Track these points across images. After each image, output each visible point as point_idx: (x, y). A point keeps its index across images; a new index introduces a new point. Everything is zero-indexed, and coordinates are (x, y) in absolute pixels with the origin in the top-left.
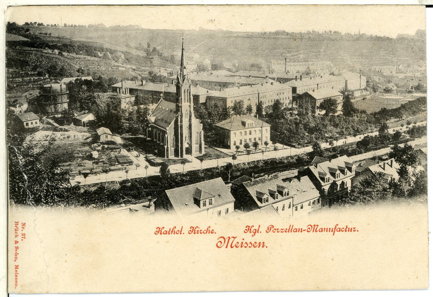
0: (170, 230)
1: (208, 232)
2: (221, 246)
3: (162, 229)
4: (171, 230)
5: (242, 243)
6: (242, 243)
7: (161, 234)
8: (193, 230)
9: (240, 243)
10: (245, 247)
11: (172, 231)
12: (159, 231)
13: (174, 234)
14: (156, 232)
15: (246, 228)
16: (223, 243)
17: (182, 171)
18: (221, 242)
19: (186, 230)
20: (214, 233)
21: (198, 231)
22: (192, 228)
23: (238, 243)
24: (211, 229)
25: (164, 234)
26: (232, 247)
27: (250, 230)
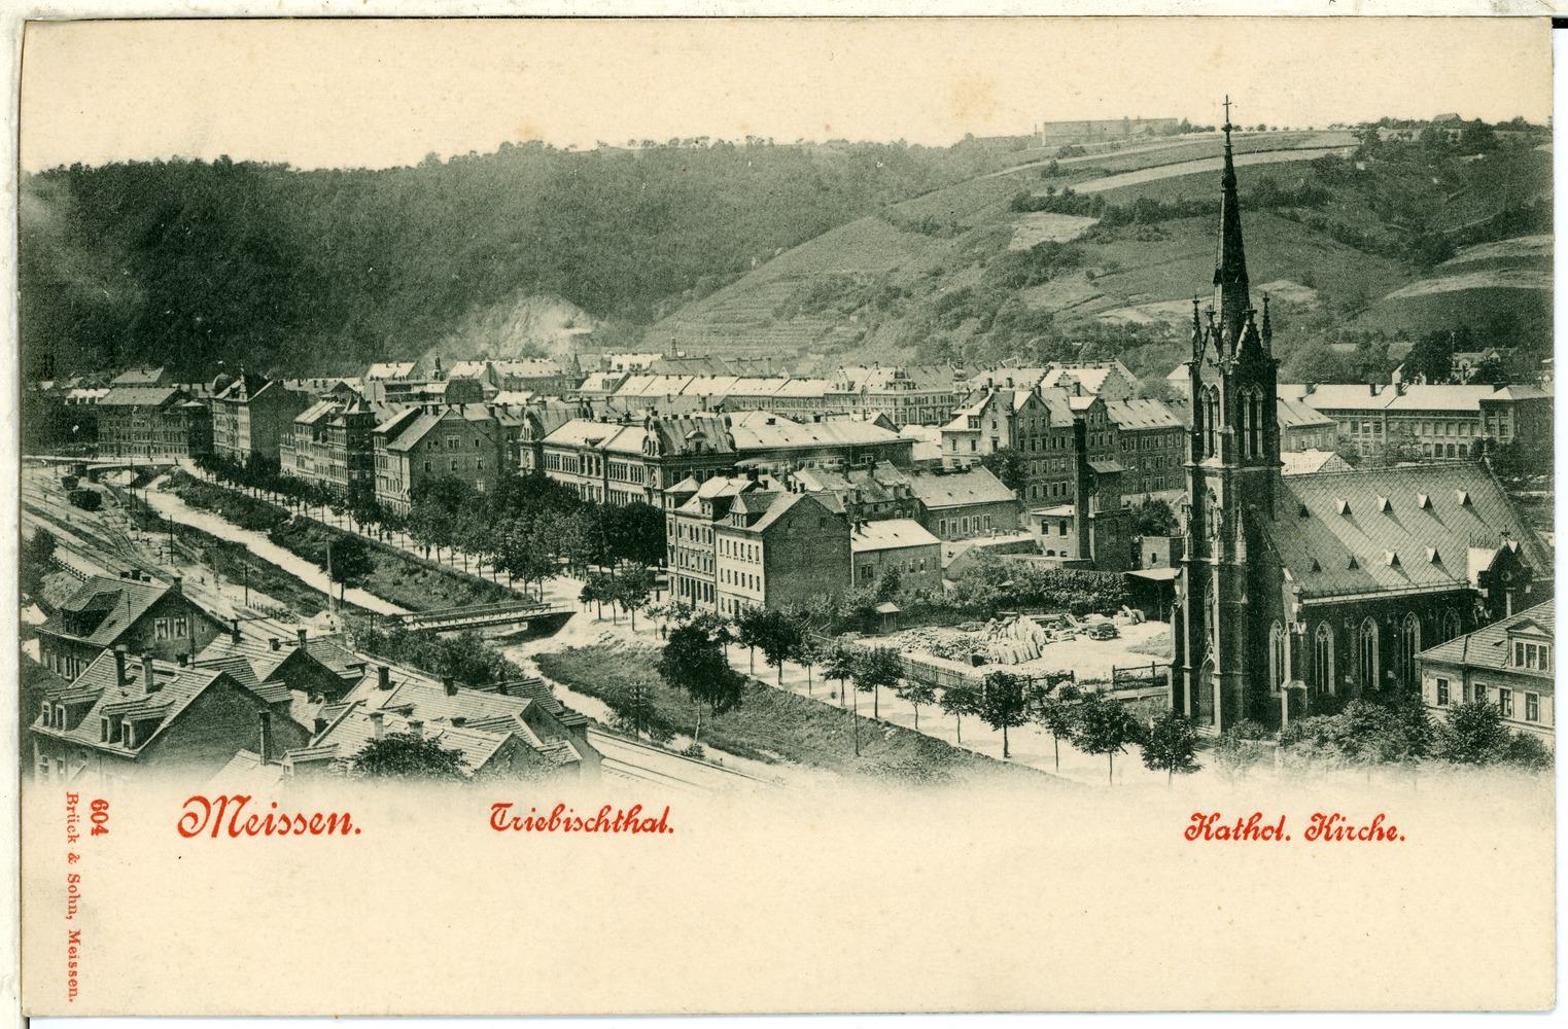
0: (1240, 824)
1: (1376, 835)
2: (192, 831)
3: (1331, 821)
4: (1245, 823)
5: (270, 818)
6: (270, 818)
7: (1207, 838)
8: (1323, 827)
9: (262, 818)
10: (282, 832)
11: (1250, 829)
12: (1201, 827)
13: (1255, 838)
14: (1190, 832)
15: (1192, 823)
16: (201, 821)
17: (1419, 781)
18: (194, 816)
19: (1296, 827)
20: (1398, 839)
21: (1340, 828)
22: (1319, 820)
23: (255, 817)
24: (1385, 826)
25: (1218, 837)
26: (233, 833)
27: (1208, 828)
